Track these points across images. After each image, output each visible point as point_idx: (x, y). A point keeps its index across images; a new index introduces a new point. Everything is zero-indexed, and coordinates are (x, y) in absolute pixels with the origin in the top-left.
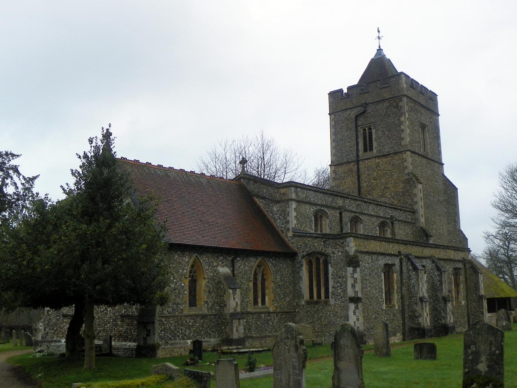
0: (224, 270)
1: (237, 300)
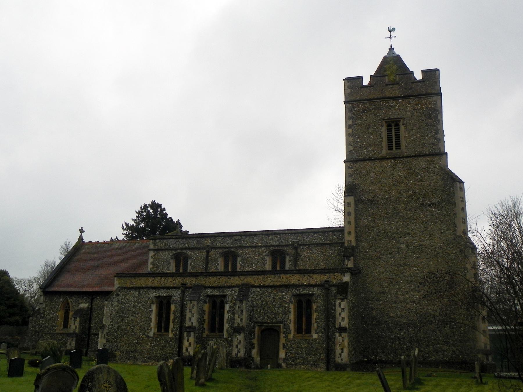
0: (84, 305)
1: (76, 324)
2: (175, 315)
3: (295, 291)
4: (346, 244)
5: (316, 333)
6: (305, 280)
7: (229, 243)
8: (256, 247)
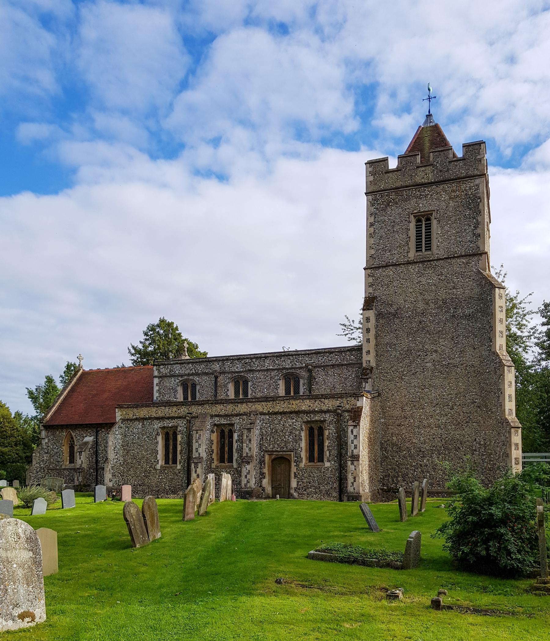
1: (82, 459)
2: (181, 446)
3: (306, 418)
4: (364, 365)
5: (329, 461)
6: (316, 405)
7: (238, 367)
8: (267, 370)
